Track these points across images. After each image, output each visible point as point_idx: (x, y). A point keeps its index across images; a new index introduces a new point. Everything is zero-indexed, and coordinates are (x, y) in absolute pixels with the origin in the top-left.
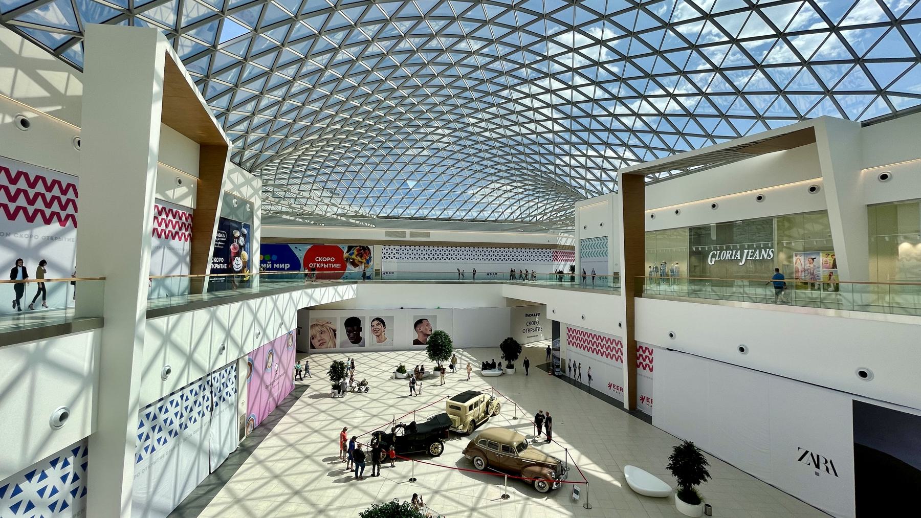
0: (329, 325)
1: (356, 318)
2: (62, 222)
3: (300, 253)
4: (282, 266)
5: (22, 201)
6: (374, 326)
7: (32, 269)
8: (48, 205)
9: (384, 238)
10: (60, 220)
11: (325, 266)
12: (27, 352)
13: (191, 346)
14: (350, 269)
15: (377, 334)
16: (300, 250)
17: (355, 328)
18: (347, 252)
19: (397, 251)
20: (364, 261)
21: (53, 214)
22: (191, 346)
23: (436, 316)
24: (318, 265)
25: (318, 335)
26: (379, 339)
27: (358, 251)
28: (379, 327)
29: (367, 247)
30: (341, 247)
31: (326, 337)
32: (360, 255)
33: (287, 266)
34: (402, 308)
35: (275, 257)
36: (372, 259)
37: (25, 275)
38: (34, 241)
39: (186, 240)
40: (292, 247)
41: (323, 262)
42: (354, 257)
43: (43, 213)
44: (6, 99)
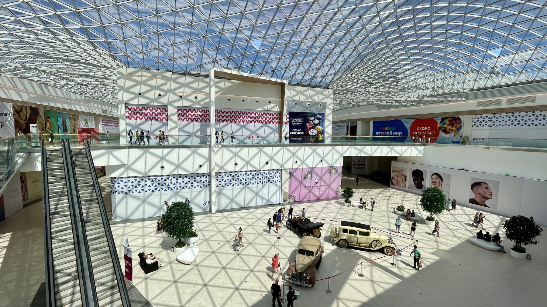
2: (227, 122)
3: (408, 125)
4: (397, 133)
5: (221, 118)
6: (433, 179)
7: (220, 133)
8: (223, 117)
9: (475, 108)
10: (226, 121)
11: (297, 133)
12: (192, 150)
14: (442, 134)
17: (419, 177)
18: (441, 123)
19: (489, 119)
20: (455, 129)
21: (224, 120)
23: (499, 182)
24: (419, 133)
25: (396, 177)
27: (449, 121)
28: (437, 181)
29: (458, 117)
30: (436, 120)
31: (400, 179)
32: (451, 124)
33: (401, 133)
34: (463, 169)
35: (394, 128)
36: (462, 127)
37: (132, 134)
38: (220, 127)
39: (276, 123)
40: (403, 121)
41: (422, 131)
42: (446, 126)
43: (222, 120)
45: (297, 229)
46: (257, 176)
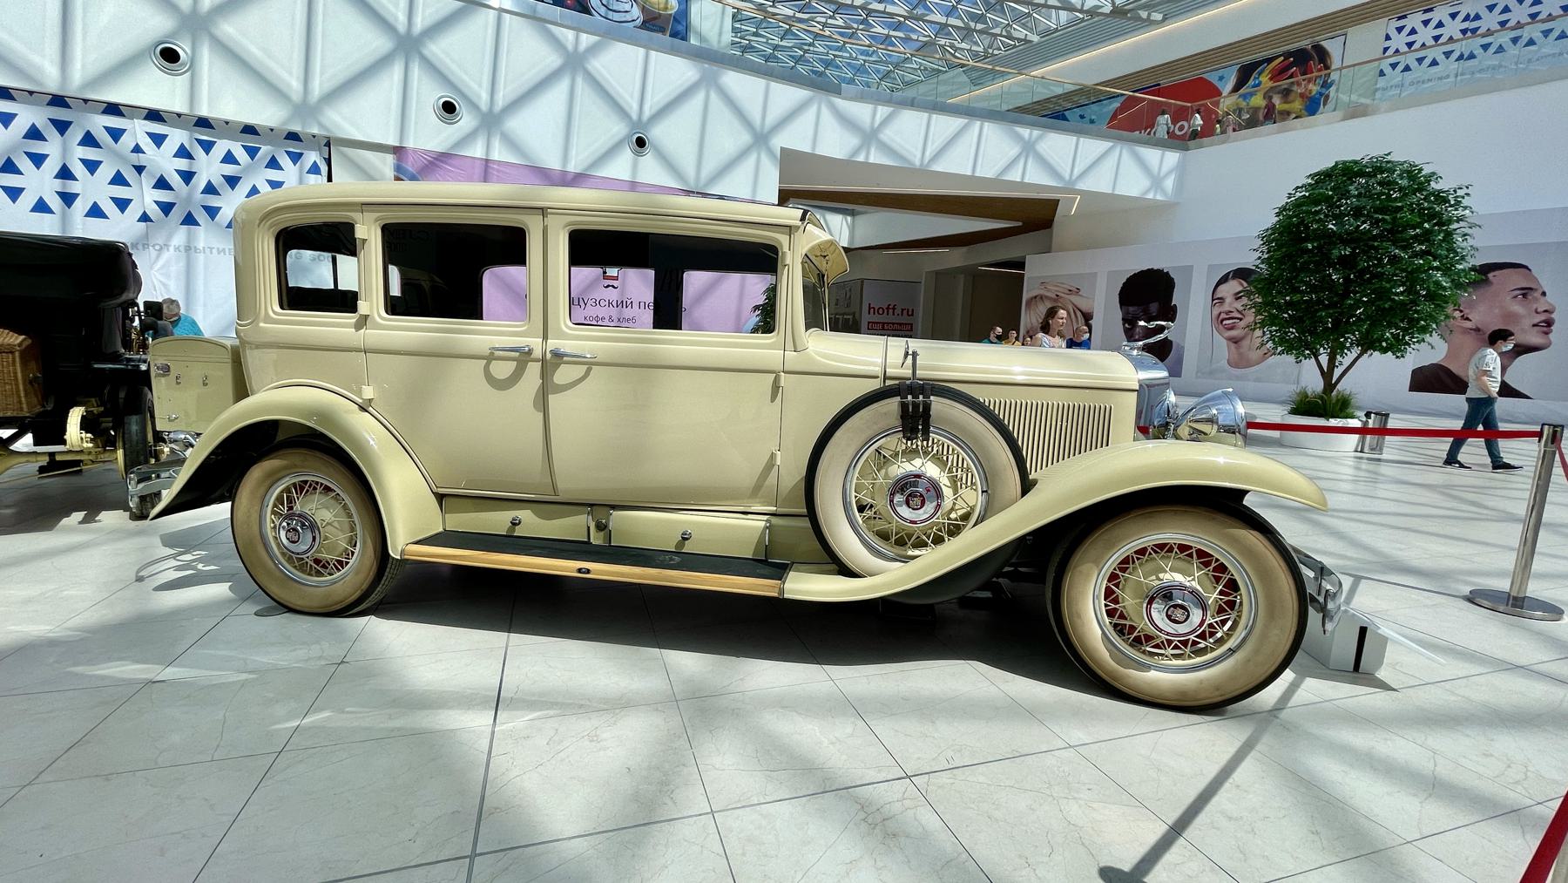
0: (1074, 298)
1: (1150, 272)
6: (1222, 300)
13: (923, 153)
15: (1233, 333)
16: (1092, 122)
18: (1236, 89)
19: (1466, 25)
22: (923, 153)
26: (1240, 355)
44: (822, 4)
45: (91, 445)
46: (147, 181)
